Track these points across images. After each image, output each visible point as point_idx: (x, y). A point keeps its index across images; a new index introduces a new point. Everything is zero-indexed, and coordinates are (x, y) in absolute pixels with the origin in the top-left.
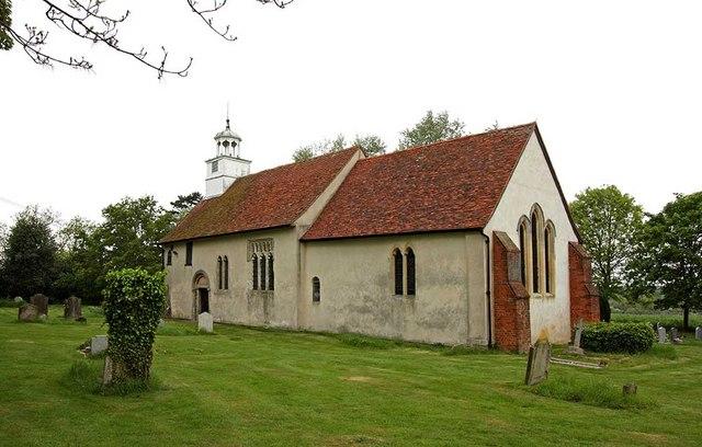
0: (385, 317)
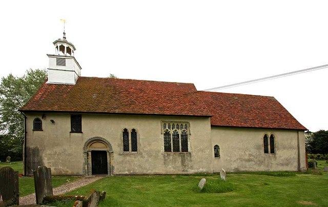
0: (261, 163)
